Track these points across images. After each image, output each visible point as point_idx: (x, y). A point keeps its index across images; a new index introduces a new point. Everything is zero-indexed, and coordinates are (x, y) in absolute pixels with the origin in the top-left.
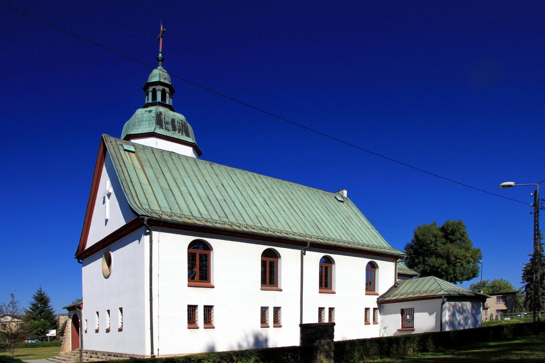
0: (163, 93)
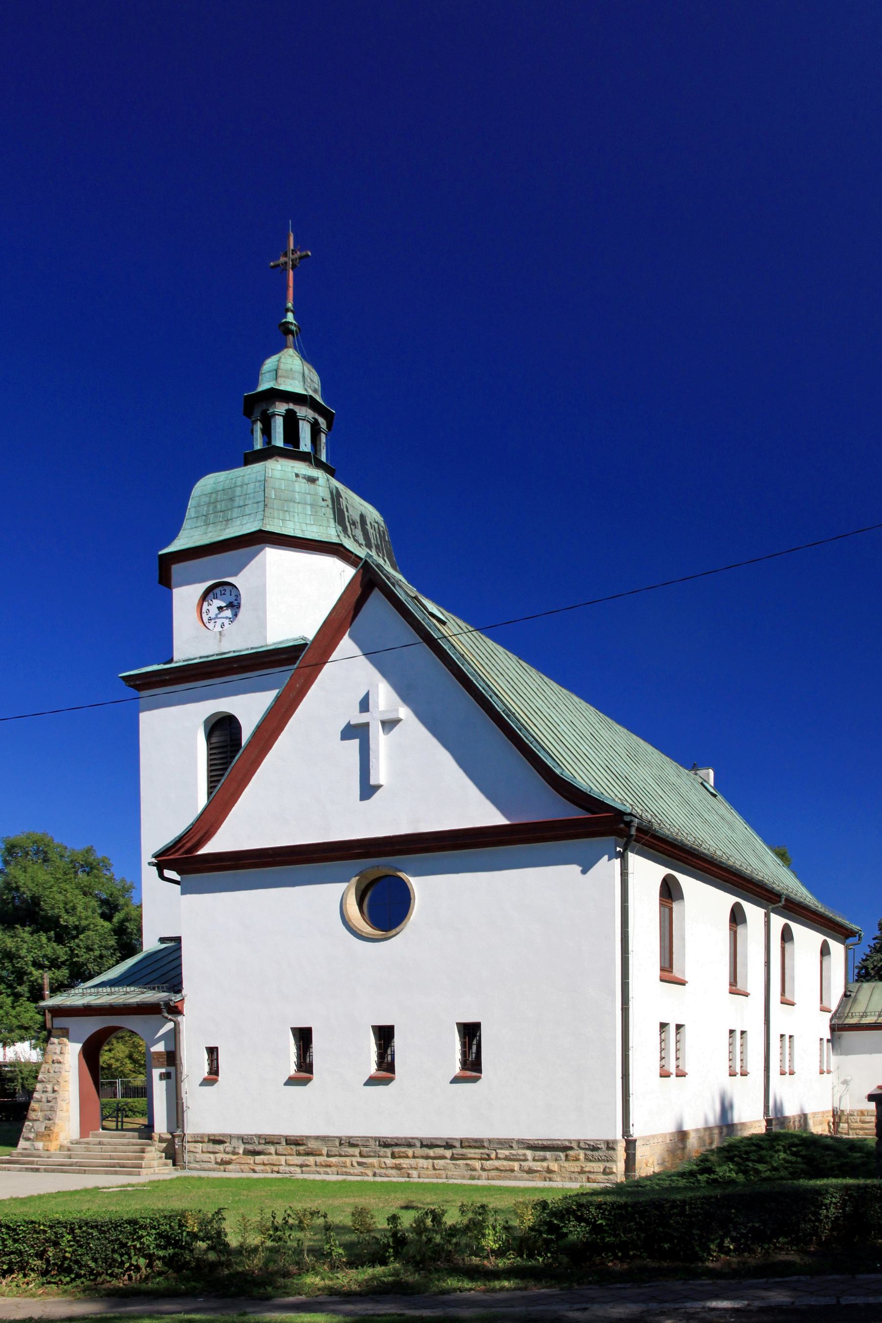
0: (291, 421)
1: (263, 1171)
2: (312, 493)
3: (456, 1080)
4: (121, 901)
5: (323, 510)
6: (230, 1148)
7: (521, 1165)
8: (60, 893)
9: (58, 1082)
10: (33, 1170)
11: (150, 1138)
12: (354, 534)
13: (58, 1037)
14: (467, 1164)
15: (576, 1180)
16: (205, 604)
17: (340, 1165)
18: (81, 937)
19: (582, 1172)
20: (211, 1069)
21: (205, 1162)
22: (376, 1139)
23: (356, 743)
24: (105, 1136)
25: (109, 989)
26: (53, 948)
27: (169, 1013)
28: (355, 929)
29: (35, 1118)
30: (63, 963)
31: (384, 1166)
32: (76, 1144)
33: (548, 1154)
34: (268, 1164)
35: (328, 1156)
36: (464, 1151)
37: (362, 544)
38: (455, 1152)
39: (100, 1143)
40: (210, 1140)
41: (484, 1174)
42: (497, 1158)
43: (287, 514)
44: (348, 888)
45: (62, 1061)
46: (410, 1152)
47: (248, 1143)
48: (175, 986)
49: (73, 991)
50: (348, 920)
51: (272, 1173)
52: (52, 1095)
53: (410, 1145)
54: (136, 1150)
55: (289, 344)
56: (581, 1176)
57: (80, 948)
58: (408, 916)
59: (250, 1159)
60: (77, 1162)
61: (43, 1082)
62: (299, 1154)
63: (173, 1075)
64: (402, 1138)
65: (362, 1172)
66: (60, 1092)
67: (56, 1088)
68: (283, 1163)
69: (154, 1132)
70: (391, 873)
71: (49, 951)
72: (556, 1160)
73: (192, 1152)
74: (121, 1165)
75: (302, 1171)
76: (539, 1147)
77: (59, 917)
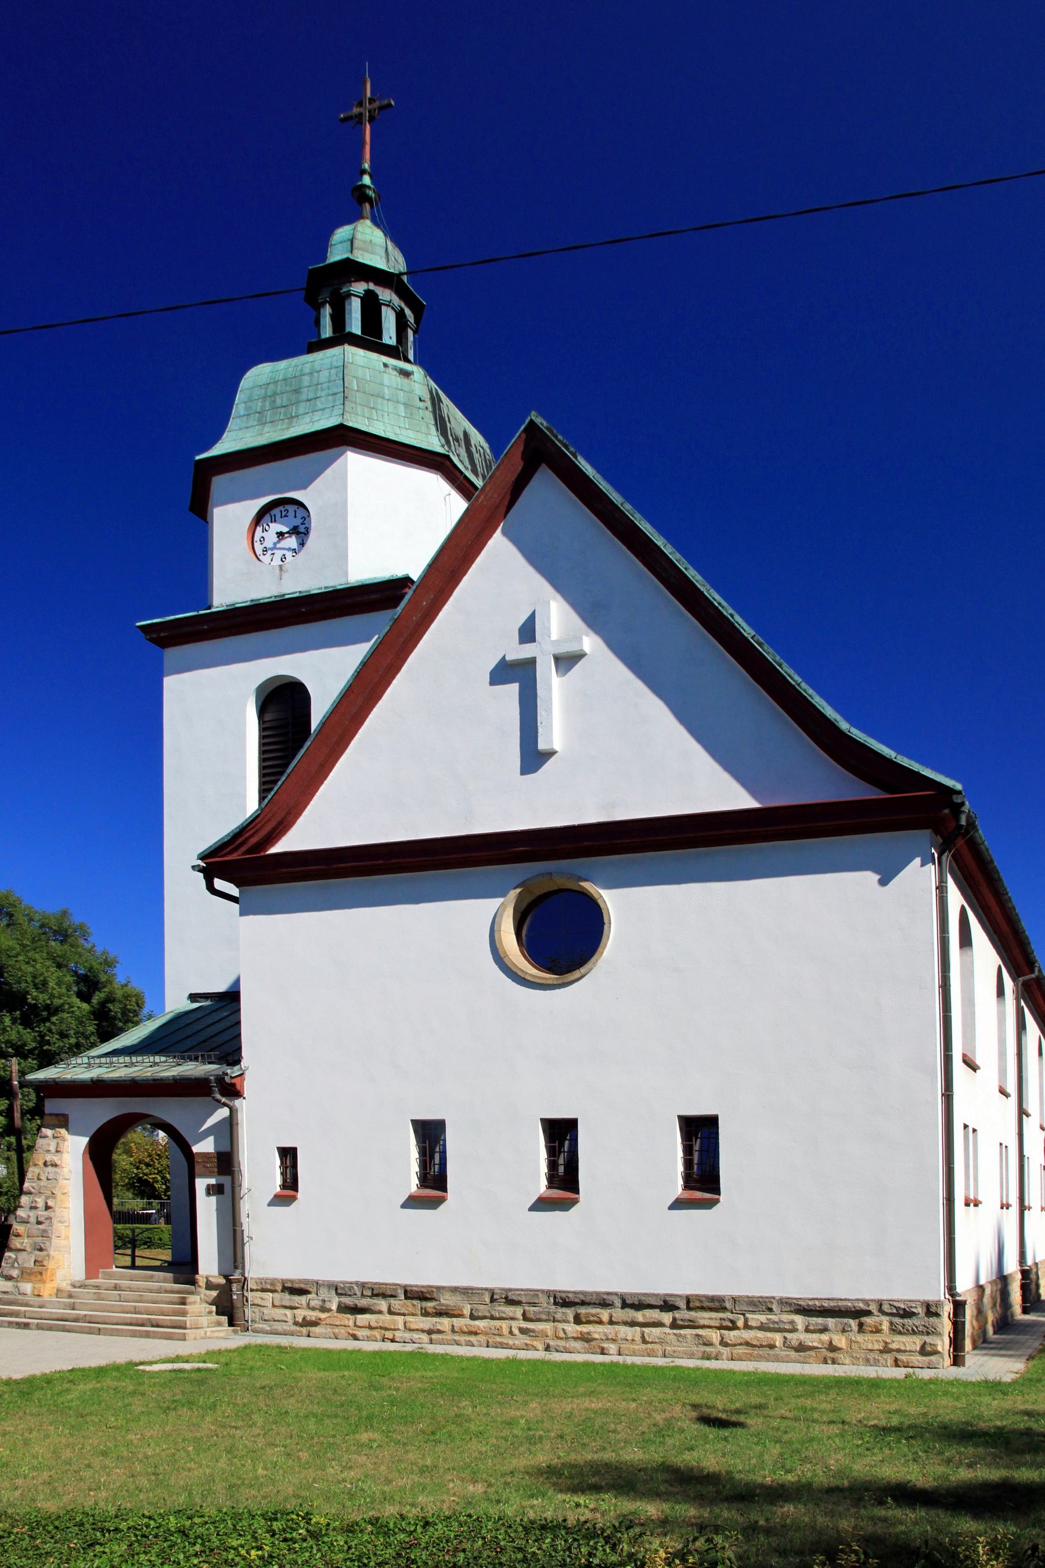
0: (371, 307)
1: (369, 1339)
2: (406, 389)
3: (678, 1204)
4: (103, 978)
5: (421, 412)
6: (316, 1302)
7: (785, 1338)
8: (28, 963)
9: (53, 1194)
10: (19, 1325)
11: (193, 1282)
13: (52, 1127)
14: (697, 1335)
15: (876, 1362)
16: (259, 529)
17: (492, 1331)
18: (54, 1019)
19: (886, 1350)
20: (284, 1180)
21: (278, 1321)
22: (548, 1293)
23: (514, 688)
24: (123, 1277)
25: (127, 1059)
26: (18, 1032)
27: (223, 1095)
28: (514, 969)
29: (19, 1246)
30: (31, 1051)
31: (563, 1335)
32: (80, 1287)
33: (831, 1322)
34: (376, 1328)
35: (473, 1317)
36: (693, 1314)
38: (677, 1316)
39: (116, 1288)
40: (285, 1289)
41: (726, 1350)
42: (747, 1326)
43: (374, 411)
44: (503, 907)
45: (58, 1162)
46: (605, 1315)
47: (345, 1294)
48: (229, 1054)
49: (73, 1061)
50: (502, 956)
51: (383, 1341)
52: (45, 1213)
53: (604, 1304)
54: (172, 1300)
55: (365, 214)
56: (885, 1356)
57: (53, 1033)
58: (600, 949)
59: (349, 1319)
60: (85, 1315)
61: (31, 1193)
62: (425, 1313)
63: (227, 1189)
64: (591, 1294)
65: (526, 1344)
66: (56, 1209)
67: (50, 1203)
68: (401, 1326)
69: (198, 1273)
70: (570, 885)
71: (13, 1036)
72: (844, 1331)
73: (258, 1305)
74: (154, 1323)
75: (431, 1340)
76: (816, 1310)
77: (28, 993)
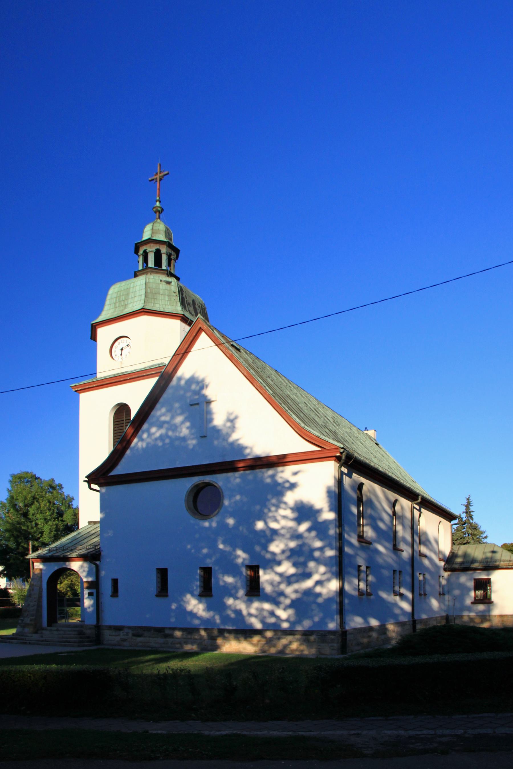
0: (158, 255)
5: (174, 298)
12: (189, 310)
37: (193, 315)
